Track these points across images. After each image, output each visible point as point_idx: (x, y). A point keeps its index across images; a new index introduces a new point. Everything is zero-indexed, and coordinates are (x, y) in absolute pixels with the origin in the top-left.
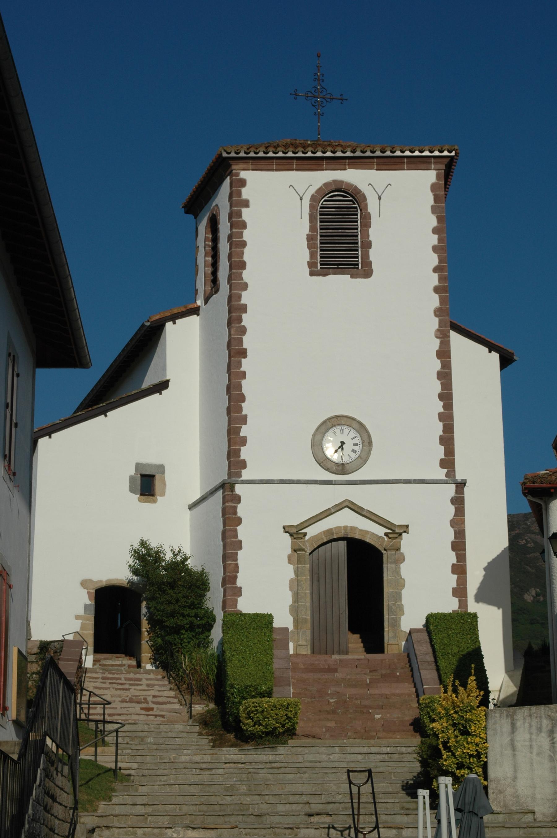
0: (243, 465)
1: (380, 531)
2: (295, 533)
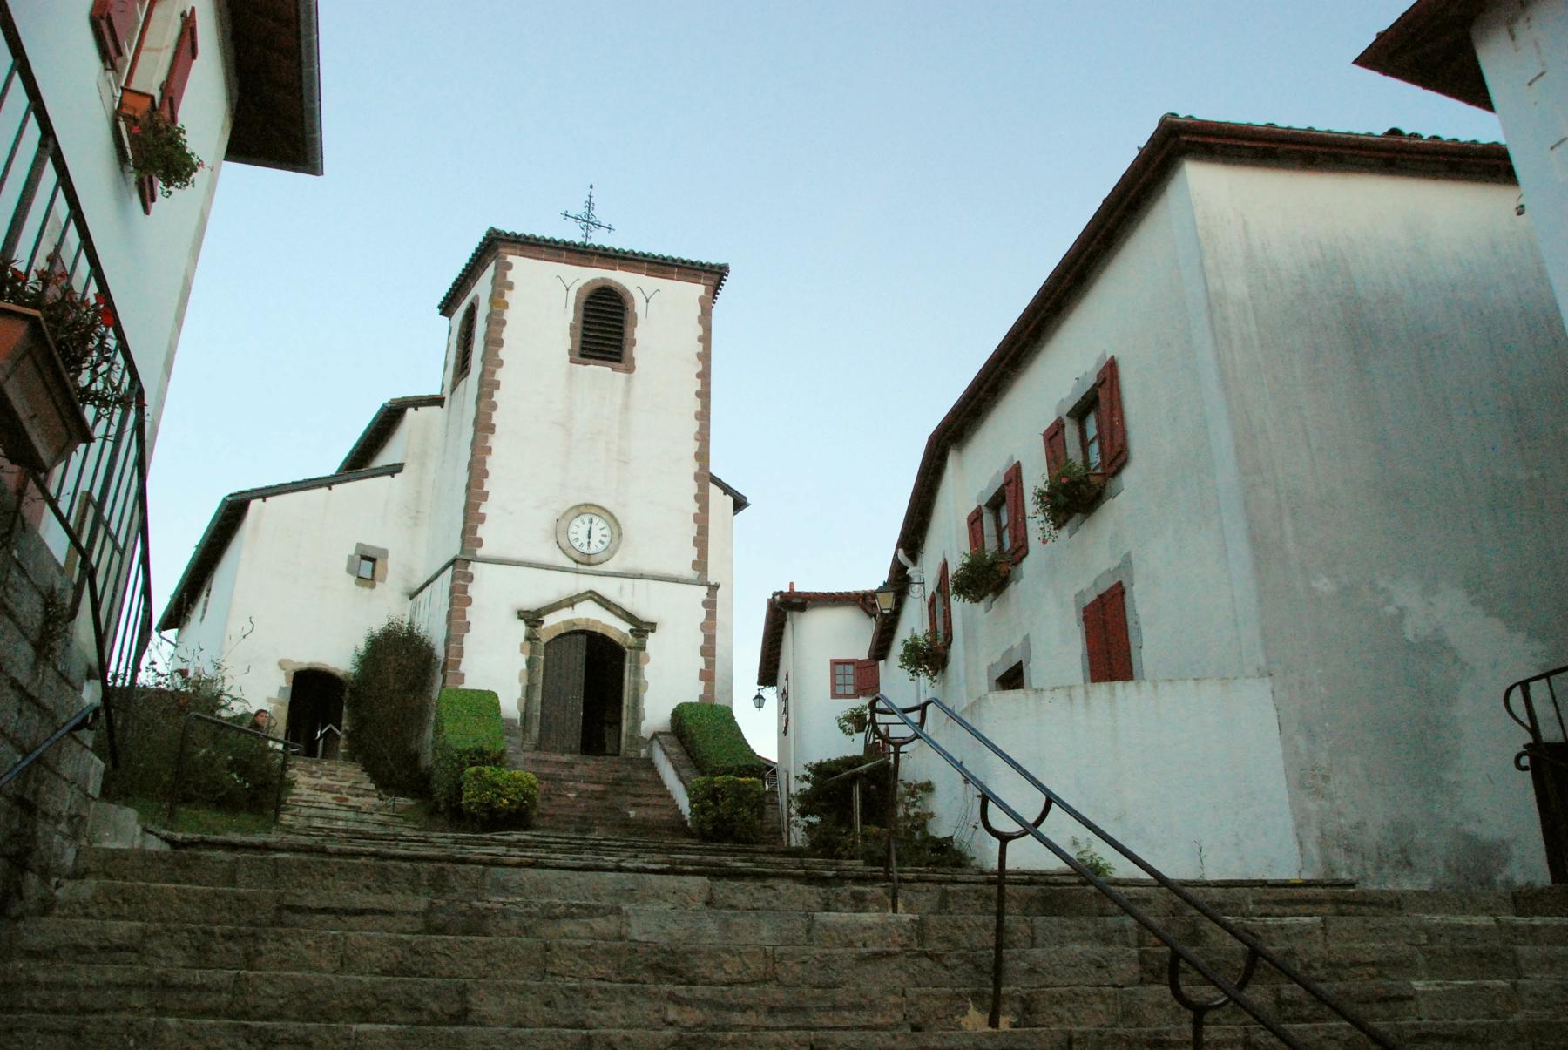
0: (480, 543)
1: (625, 628)
2: (532, 619)
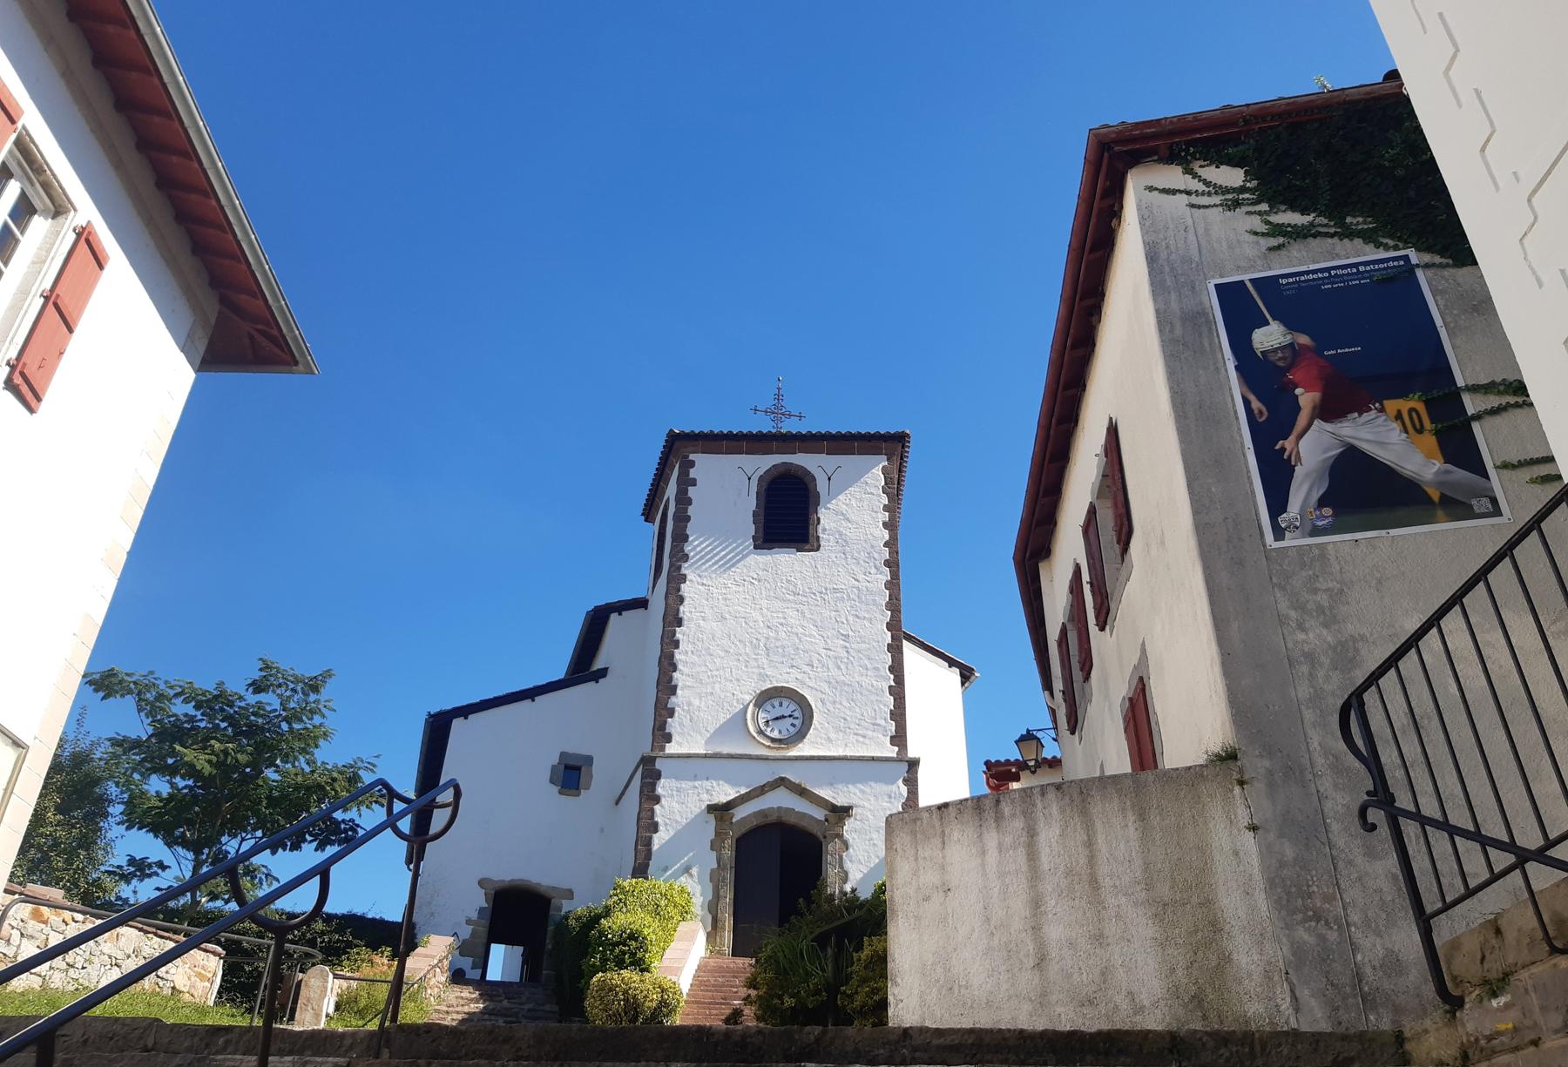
2: (720, 811)
